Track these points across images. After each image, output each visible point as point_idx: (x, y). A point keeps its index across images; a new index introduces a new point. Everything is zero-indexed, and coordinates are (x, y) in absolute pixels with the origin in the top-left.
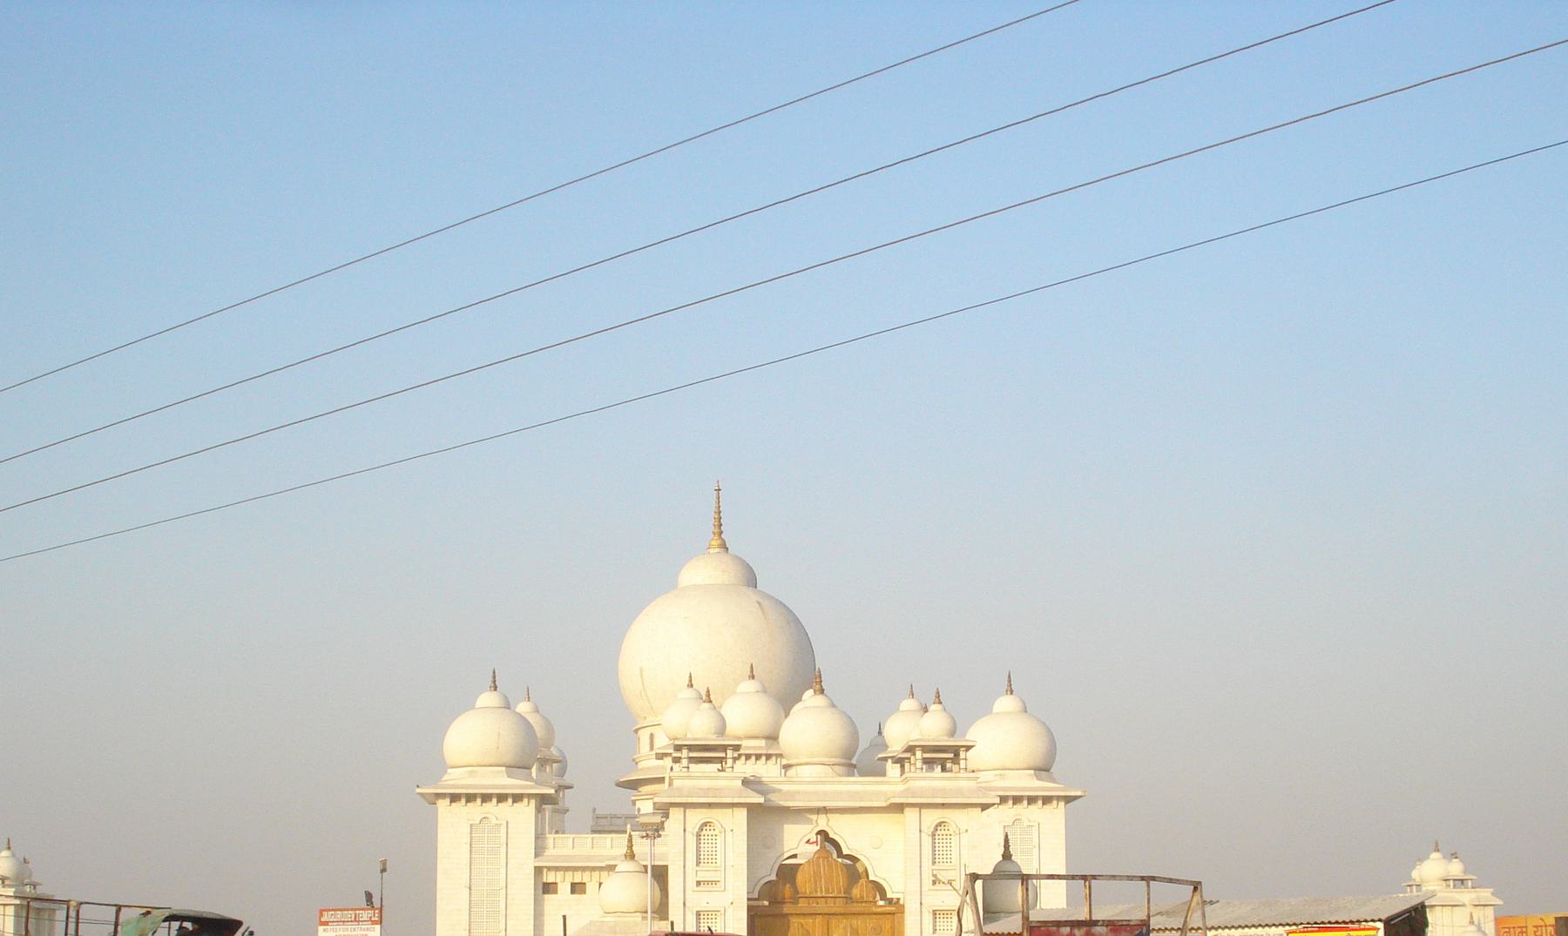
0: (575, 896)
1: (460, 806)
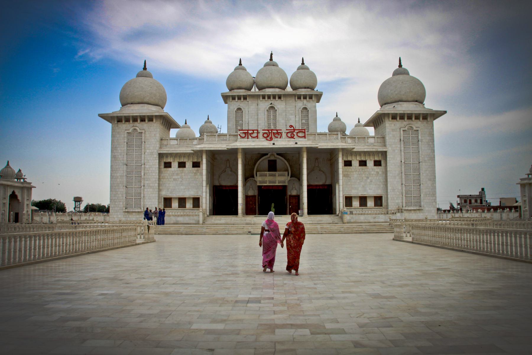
0: (181, 169)
1: (399, 124)
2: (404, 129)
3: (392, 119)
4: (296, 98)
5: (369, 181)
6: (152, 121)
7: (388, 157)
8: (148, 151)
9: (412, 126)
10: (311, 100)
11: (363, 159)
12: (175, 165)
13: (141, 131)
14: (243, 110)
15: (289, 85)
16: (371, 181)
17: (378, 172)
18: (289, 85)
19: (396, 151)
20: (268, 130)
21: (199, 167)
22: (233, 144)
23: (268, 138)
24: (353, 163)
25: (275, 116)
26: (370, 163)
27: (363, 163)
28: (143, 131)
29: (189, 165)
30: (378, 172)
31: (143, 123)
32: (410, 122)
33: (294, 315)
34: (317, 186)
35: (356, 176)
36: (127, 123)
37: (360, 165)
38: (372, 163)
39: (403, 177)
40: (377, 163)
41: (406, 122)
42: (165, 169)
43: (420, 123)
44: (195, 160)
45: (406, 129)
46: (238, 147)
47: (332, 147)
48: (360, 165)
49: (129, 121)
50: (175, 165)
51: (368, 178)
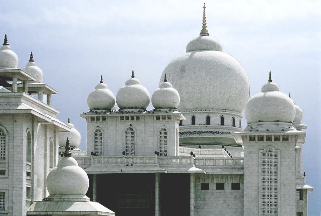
4: (155, 118)
7: (245, 180)
9: (272, 148)
10: (170, 120)
12: (212, 187)
14: (167, 130)
15: (116, 104)
18: (116, 104)
25: (133, 137)
26: (228, 187)
27: (220, 186)
28: (278, 151)
32: (269, 143)
38: (215, 186)
39: (260, 202)
40: (236, 187)
41: (265, 143)
42: (203, 191)
43: (280, 144)
45: (265, 150)
46: (156, 172)
47: (133, 172)
50: (212, 187)
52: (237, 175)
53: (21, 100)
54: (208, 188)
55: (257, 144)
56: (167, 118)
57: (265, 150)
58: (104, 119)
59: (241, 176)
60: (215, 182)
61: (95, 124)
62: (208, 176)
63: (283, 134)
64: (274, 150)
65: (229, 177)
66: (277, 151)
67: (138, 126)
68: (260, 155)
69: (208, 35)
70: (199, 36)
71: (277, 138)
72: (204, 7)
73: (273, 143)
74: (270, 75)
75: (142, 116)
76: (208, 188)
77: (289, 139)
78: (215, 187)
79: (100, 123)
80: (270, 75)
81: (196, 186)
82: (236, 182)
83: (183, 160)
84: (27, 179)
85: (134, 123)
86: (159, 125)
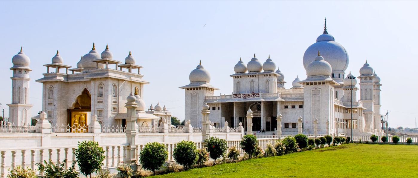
2: (312, 90)
3: (315, 84)
5: (296, 115)
6: (325, 84)
8: (199, 103)
11: (293, 105)
13: (319, 89)
16: (297, 116)
17: (301, 111)
19: (309, 101)
20: (245, 94)
21: (302, 108)
22: (276, 99)
23: (245, 98)
24: (289, 107)
27: (293, 107)
29: (297, 107)
30: (301, 111)
31: (320, 85)
32: (316, 86)
33: (257, 162)
34: (221, 114)
35: (290, 113)
36: (312, 85)
37: (292, 108)
41: (314, 86)
44: (293, 105)
45: (314, 89)
48: (292, 108)
49: (317, 84)
51: (296, 114)
52: (301, 102)
53: (108, 74)
54: (287, 108)
55: (310, 87)
56: (268, 76)
57: (314, 89)
58: (241, 77)
59: (303, 102)
60: (291, 105)
61: (237, 79)
62: (288, 102)
63: (323, 81)
64: (318, 89)
65: (293, 103)
66: (319, 89)
67: (256, 79)
68: (311, 91)
69: (327, 33)
70: (92, 49)
71: (320, 83)
72: (325, 19)
73: (318, 86)
74: (200, 62)
75: (272, 74)
76: (287, 108)
77: (202, 89)
78: (291, 107)
79: (239, 79)
80: (200, 62)
81: (281, 108)
82: (301, 105)
83: (227, 96)
84: (336, 106)
85: (254, 78)
86: (266, 78)
